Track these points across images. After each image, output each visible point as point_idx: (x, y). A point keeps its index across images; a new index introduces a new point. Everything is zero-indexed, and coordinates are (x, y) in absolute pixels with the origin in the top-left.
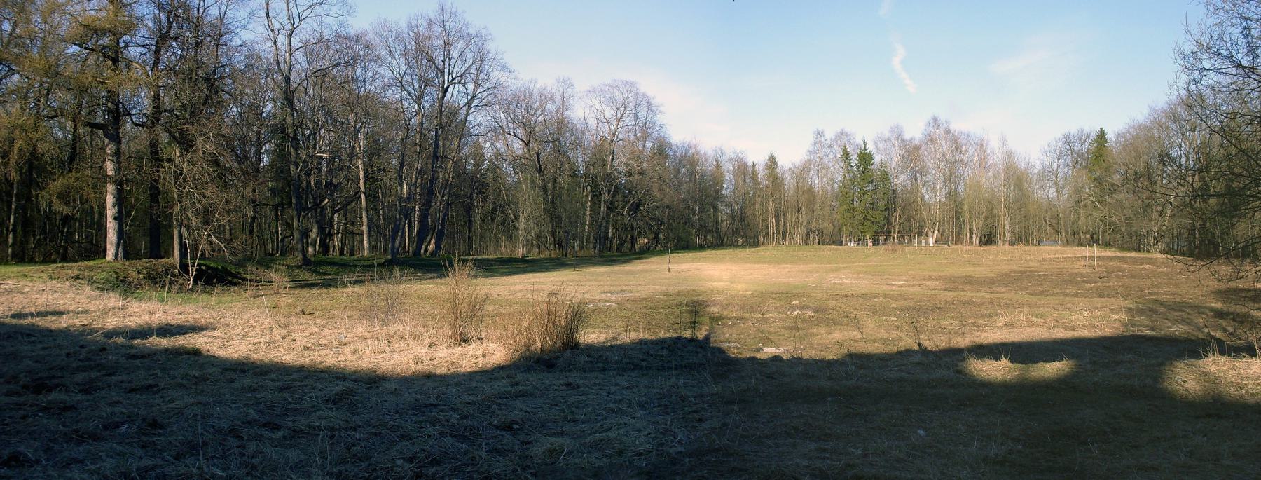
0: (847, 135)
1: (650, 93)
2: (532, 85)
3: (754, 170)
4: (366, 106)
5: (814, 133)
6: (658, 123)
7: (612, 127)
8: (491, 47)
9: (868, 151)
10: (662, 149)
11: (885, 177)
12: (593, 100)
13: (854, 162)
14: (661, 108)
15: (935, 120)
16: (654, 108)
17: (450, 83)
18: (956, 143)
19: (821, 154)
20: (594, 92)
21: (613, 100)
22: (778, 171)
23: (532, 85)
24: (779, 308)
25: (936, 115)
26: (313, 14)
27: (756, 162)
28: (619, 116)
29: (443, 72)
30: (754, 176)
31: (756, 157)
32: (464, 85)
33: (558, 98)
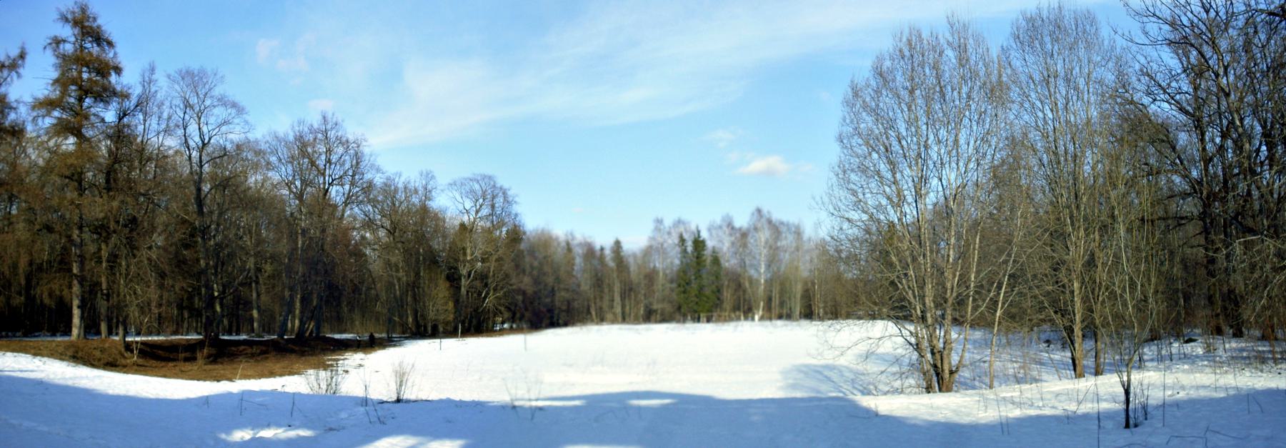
0: (684, 223)
1: (506, 186)
4: (254, 202)
5: (654, 221)
7: (471, 217)
8: (366, 150)
9: (701, 239)
10: (516, 235)
11: (716, 261)
12: (454, 192)
13: (690, 249)
14: (516, 199)
15: (759, 211)
16: (510, 199)
18: (776, 229)
19: (660, 240)
20: (455, 185)
21: (473, 191)
22: (622, 254)
25: (760, 207)
27: (604, 246)
28: (478, 207)
29: (323, 175)
30: (602, 257)
31: (603, 240)
32: (342, 185)
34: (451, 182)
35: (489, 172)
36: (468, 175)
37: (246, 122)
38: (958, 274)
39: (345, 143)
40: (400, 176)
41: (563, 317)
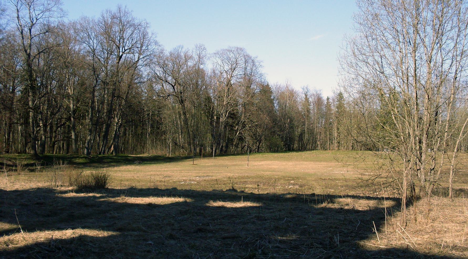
2: (180, 49)
3: (328, 102)
6: (259, 73)
8: (149, 31)
12: (217, 59)
14: (261, 64)
17: (123, 53)
20: (218, 53)
23: (180, 49)
24: (282, 185)
26: (44, 16)
30: (328, 105)
33: (196, 57)
34: (215, 52)
35: (240, 45)
36: (226, 47)
37: (61, 10)
38: (72, 88)
39: (136, 27)
40: (182, 47)
41: (309, 146)
